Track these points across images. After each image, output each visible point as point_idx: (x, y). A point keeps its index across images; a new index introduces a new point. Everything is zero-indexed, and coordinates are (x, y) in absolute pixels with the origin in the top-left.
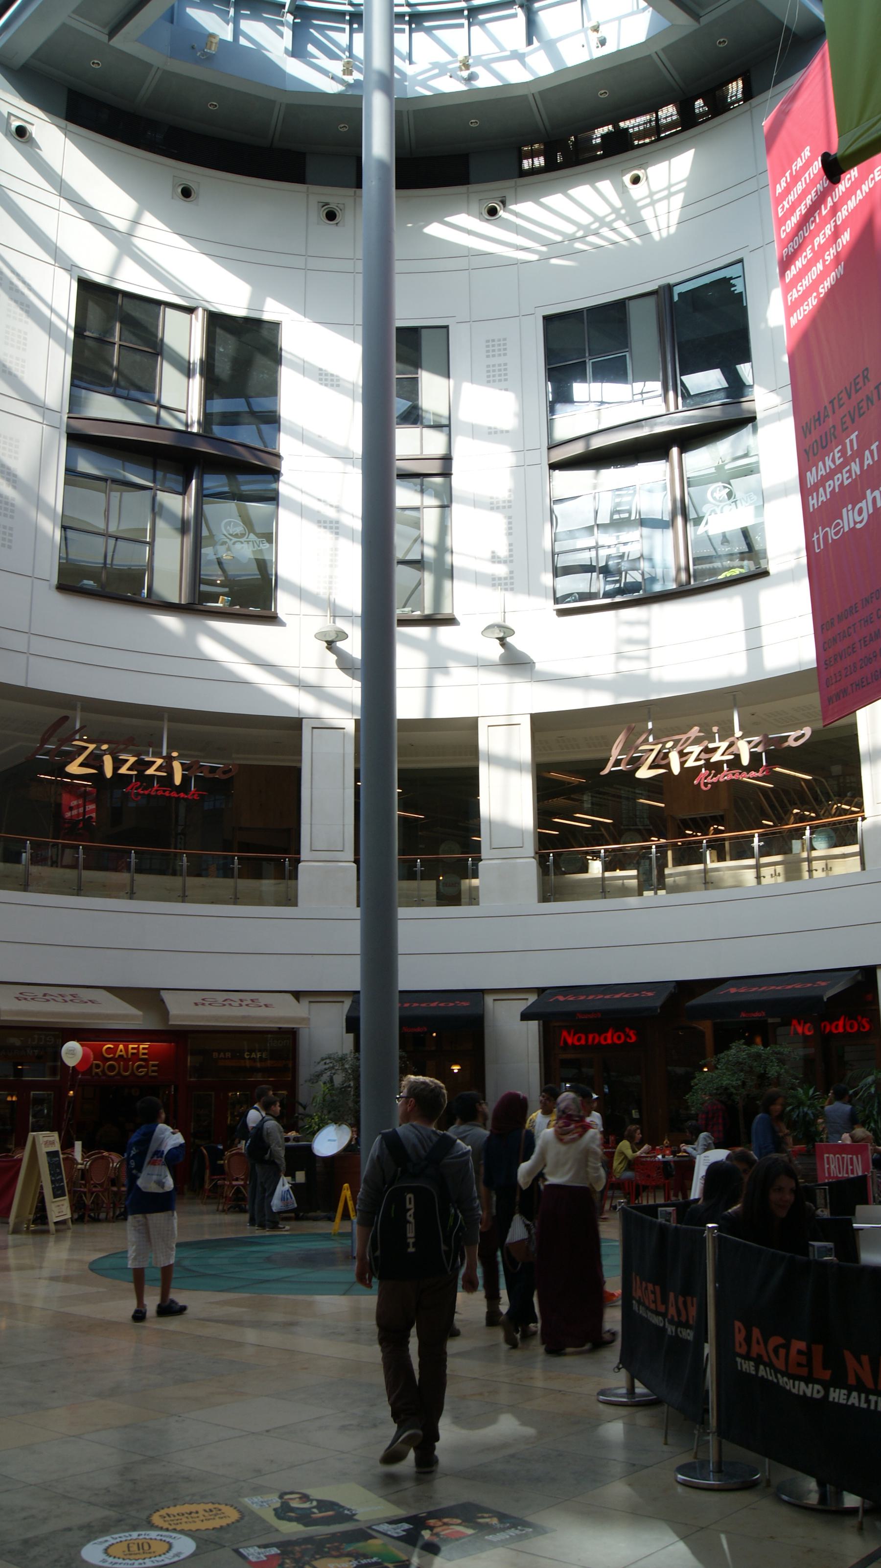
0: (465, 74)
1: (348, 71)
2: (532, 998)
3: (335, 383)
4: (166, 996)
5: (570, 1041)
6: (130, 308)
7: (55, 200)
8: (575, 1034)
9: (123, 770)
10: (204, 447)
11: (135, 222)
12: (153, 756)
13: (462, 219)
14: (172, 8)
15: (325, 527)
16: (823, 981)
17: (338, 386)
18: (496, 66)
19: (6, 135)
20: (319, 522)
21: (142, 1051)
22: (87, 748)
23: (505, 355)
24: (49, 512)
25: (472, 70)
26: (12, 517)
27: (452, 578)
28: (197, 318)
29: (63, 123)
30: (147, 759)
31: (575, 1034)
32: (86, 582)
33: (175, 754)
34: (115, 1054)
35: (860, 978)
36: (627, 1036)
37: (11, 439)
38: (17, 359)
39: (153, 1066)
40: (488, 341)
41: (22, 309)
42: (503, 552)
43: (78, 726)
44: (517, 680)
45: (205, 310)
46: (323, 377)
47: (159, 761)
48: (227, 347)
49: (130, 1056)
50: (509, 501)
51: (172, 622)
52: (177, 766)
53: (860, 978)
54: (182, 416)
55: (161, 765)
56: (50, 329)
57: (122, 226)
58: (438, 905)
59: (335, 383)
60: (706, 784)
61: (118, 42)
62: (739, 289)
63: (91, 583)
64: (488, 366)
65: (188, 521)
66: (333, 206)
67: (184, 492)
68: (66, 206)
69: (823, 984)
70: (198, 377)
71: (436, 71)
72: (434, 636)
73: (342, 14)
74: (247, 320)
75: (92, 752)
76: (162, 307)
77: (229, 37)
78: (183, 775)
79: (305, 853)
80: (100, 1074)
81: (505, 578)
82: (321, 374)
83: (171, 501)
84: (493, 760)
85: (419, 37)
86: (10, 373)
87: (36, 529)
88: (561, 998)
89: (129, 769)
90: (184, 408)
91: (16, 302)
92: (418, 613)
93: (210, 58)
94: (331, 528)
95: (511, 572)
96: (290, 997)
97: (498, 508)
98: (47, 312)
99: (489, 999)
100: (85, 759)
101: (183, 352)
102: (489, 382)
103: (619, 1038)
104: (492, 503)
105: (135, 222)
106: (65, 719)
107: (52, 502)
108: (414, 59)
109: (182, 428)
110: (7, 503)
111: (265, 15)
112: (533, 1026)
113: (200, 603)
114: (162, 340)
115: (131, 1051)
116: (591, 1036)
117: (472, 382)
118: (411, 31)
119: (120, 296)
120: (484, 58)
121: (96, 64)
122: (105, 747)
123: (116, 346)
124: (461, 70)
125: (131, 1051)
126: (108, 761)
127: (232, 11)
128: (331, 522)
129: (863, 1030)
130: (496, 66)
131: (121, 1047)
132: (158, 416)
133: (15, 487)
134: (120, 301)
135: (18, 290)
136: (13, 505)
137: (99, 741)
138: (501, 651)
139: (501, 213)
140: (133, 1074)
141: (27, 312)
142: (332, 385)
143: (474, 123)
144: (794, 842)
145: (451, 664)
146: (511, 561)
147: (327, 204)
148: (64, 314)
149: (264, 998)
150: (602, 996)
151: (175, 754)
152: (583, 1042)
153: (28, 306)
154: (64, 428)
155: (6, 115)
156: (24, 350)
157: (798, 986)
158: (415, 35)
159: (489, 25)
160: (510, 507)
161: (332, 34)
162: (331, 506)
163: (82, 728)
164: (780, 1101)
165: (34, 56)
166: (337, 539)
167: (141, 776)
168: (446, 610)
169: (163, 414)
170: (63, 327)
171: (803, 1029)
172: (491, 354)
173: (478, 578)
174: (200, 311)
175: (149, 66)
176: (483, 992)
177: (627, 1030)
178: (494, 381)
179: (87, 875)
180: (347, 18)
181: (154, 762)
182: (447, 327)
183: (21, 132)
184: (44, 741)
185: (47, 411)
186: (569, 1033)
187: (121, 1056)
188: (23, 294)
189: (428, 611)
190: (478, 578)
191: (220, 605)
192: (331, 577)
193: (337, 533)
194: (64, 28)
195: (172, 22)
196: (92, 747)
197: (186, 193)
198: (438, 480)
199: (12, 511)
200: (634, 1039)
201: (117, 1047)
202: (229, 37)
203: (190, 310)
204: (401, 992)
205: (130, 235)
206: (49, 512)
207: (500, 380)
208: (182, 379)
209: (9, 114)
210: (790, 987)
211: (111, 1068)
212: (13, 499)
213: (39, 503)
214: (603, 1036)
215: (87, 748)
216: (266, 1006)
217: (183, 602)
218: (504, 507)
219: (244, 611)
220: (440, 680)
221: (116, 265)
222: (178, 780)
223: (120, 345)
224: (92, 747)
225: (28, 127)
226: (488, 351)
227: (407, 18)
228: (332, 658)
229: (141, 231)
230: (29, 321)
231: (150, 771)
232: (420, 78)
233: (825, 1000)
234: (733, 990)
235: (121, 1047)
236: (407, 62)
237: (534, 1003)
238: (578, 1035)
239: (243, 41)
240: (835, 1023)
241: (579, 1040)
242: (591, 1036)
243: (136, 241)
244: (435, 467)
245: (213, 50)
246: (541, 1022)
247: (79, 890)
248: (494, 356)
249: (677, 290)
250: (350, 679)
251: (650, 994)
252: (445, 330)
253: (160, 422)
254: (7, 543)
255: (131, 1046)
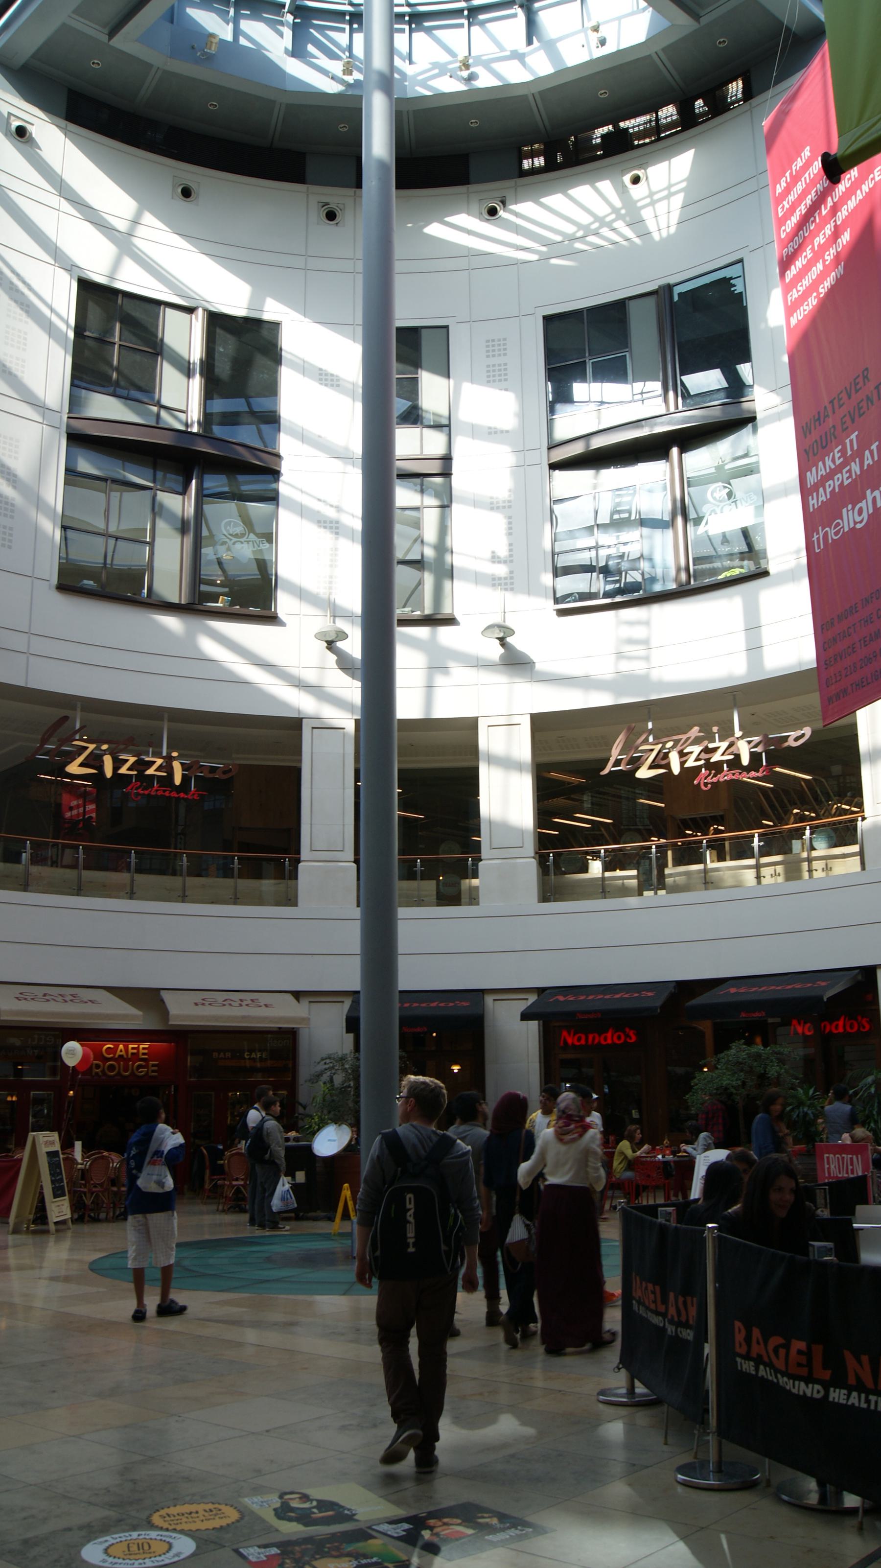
0: (465, 74)
1: (348, 71)
2: (532, 998)
3: (335, 383)
4: (166, 996)
5: (570, 1041)
6: (130, 308)
7: (55, 200)
8: (575, 1034)
9: (123, 770)
10: (204, 447)
11: (135, 222)
12: (153, 756)
13: (462, 219)
14: (172, 8)
15: (325, 527)
16: (823, 981)
17: (338, 386)
18: (496, 66)
19: (6, 135)
20: (319, 522)
21: (142, 1051)
22: (87, 748)
23: (505, 355)
24: (49, 512)
25: (472, 70)
26: (12, 517)
27: (452, 578)
28: (197, 318)
29: (63, 123)
30: (147, 759)
31: (575, 1034)
32: (86, 582)
33: (175, 754)
34: (115, 1054)
35: (860, 978)
36: (627, 1036)
37: (11, 439)
38: (17, 359)
39: (153, 1066)
40: (488, 341)
41: (22, 309)
42: (503, 552)
43: (78, 726)
44: (517, 680)
45: (205, 310)
46: (323, 377)
47: (159, 761)
48: (227, 347)
49: (130, 1056)
50: (509, 501)
51: (172, 622)
52: (177, 766)
53: (860, 978)
54: (182, 416)
55: (161, 765)
56: (50, 329)
57: (122, 226)
58: (438, 905)
59: (335, 383)
60: (706, 784)
61: (118, 42)
62: (739, 289)
63: (91, 583)
64: (488, 366)
65: (188, 521)
66: (333, 206)
67: (184, 492)
68: (66, 206)
69: (823, 984)
70: (198, 377)
71: (436, 71)
72: (434, 636)
73: (342, 14)
74: (247, 320)
75: (92, 752)
76: (162, 307)
77: (229, 37)
78: (183, 775)
79: (305, 853)
80: (100, 1074)
81: (505, 578)
82: (321, 374)
83: (171, 501)
84: (493, 760)
85: (419, 37)
86: (10, 373)
87: (36, 529)
88: (561, 998)
89: (129, 769)
90: (184, 408)
91: (16, 302)
92: (418, 613)
93: (210, 58)
94: (331, 528)
95: (511, 572)
96: (290, 997)
97: (498, 508)
98: (47, 312)
99: (489, 999)
100: (85, 759)
101: (183, 352)
102: (489, 382)
103: (619, 1038)
104: (492, 503)
105: (135, 222)
106: (65, 719)
107: (52, 502)
108: (414, 59)
109: (182, 428)
110: (7, 503)
111: (265, 15)
112: (533, 1026)
113: (200, 603)
114: (162, 340)
115: (131, 1051)
116: (591, 1036)
117: (472, 382)
118: (411, 31)
119: (120, 296)
120: (484, 58)
121: (96, 64)
122: (105, 747)
123: (116, 346)
124: (461, 70)
125: (131, 1051)
126: (108, 761)
127: (232, 11)
128: (331, 522)
129: (863, 1030)
130: (496, 66)
131: (121, 1047)
132: (158, 416)
133: (15, 487)
134: (120, 301)
135: (18, 290)
136: (13, 505)
137: (99, 741)
138: (501, 651)
139: (501, 213)
140: (133, 1074)
141: (27, 312)
142: (332, 385)
143: (474, 123)
144: (794, 842)
145: (451, 664)
146: (511, 561)
147: (327, 204)
148: (64, 314)
149: (264, 998)
150: (602, 996)
151: (175, 754)
152: (583, 1042)
153: (28, 306)
154: (64, 428)
155: (6, 115)
156: (24, 350)
157: (798, 986)
158: (415, 35)
159: (489, 25)
160: (510, 507)
161: (332, 34)
162: (331, 506)
163: (82, 728)
164: (780, 1101)
165: (34, 56)
166: (337, 539)
167: (141, 776)
168: (446, 610)
169: (163, 414)
170: (63, 327)
171: (803, 1029)
172: (491, 354)
173: (478, 578)
174: (200, 311)
175: (149, 66)
176: (483, 992)
177: (627, 1030)
178: (494, 381)
179: (87, 875)
180: (347, 18)
181: (154, 762)
182: (447, 327)
183: (21, 132)
184: (44, 741)
185: (47, 411)
186: (569, 1033)
187: (121, 1056)
188: (23, 294)
189: (428, 611)
190: (478, 578)
191: (220, 605)
192: (331, 577)
193: (337, 533)
194: (64, 28)
195: (172, 22)
196: (92, 747)
197: (186, 193)
198: (438, 480)
199: (12, 511)
200: (634, 1039)
201: (117, 1047)
202: (229, 37)
203: (190, 310)
204: (401, 992)
205: (130, 235)
206: (49, 512)
207: (500, 380)
208: (182, 379)
209: (9, 114)
210: (790, 987)
211: (111, 1068)
212: (13, 499)
213: (39, 503)
214: (603, 1036)
215: (87, 748)
216: (266, 1006)
217: (183, 602)
218: (504, 507)
219: (244, 611)
220: (440, 680)
221: (116, 265)
222: (178, 780)
223: (120, 345)
224: (92, 747)
225: (28, 127)
226: (488, 351)
227: (407, 18)
228: (332, 658)
229: (141, 231)
230: (29, 321)
231: (150, 771)
232: (420, 78)
233: (825, 1000)
234: (733, 990)
235: (121, 1047)
236: (407, 62)
237: (534, 1003)
238: (578, 1035)
239: (243, 41)
240: (835, 1023)
241: (579, 1040)
242: (591, 1036)
243: (136, 241)
244: (435, 467)
245: (213, 50)
246: (541, 1022)
247: (79, 890)
248: (494, 356)
249: (677, 290)
250: (350, 679)
251: (650, 994)
252: (445, 330)
253: (160, 422)
254: (7, 543)
255: (131, 1046)
